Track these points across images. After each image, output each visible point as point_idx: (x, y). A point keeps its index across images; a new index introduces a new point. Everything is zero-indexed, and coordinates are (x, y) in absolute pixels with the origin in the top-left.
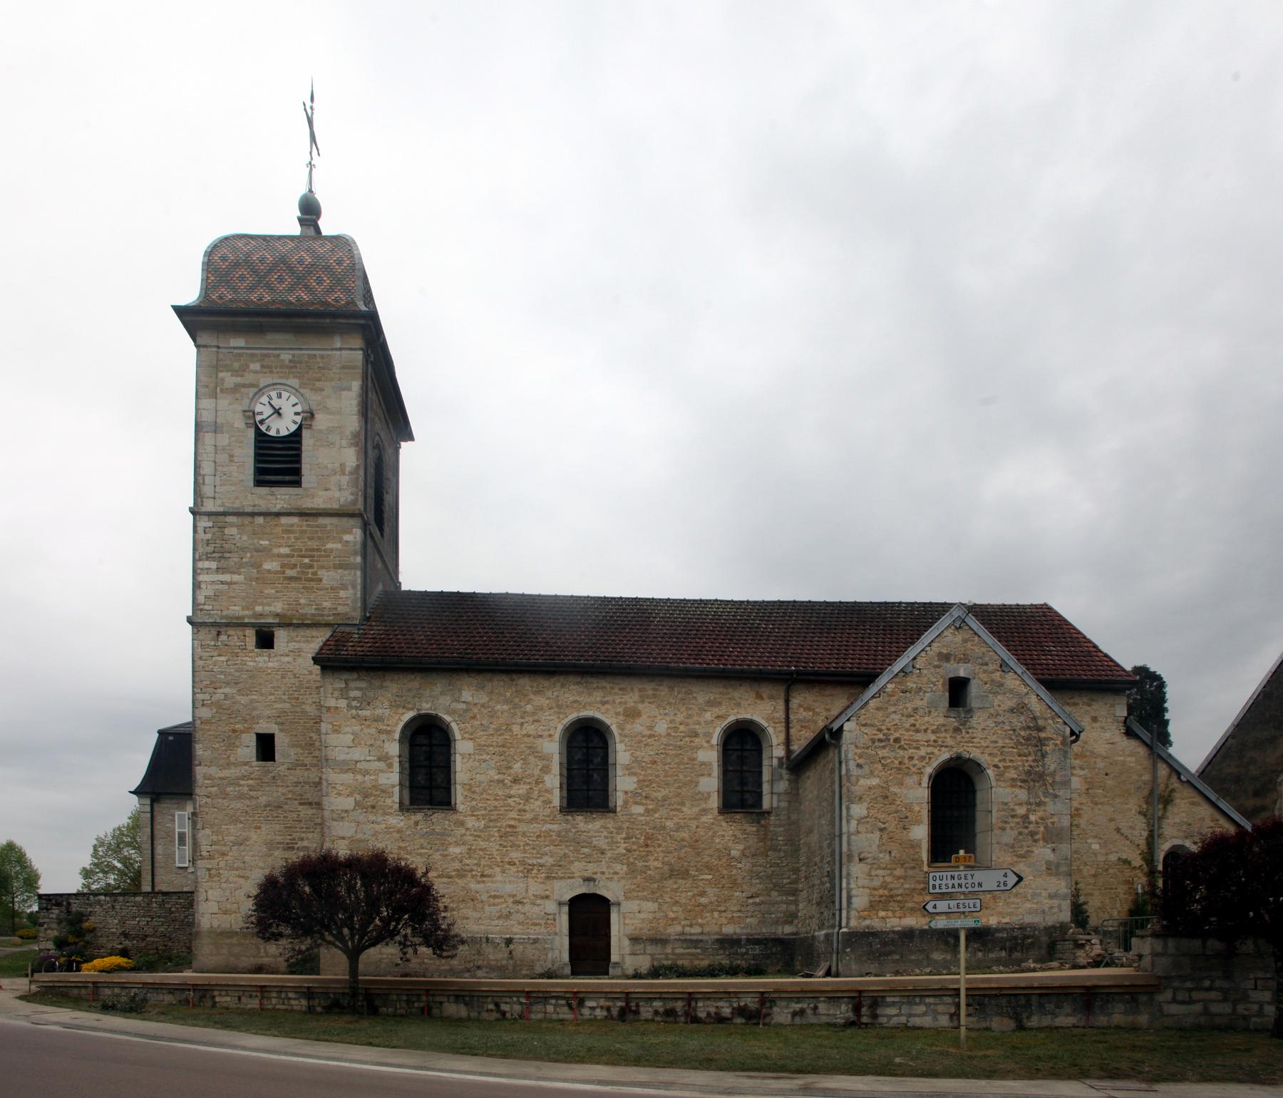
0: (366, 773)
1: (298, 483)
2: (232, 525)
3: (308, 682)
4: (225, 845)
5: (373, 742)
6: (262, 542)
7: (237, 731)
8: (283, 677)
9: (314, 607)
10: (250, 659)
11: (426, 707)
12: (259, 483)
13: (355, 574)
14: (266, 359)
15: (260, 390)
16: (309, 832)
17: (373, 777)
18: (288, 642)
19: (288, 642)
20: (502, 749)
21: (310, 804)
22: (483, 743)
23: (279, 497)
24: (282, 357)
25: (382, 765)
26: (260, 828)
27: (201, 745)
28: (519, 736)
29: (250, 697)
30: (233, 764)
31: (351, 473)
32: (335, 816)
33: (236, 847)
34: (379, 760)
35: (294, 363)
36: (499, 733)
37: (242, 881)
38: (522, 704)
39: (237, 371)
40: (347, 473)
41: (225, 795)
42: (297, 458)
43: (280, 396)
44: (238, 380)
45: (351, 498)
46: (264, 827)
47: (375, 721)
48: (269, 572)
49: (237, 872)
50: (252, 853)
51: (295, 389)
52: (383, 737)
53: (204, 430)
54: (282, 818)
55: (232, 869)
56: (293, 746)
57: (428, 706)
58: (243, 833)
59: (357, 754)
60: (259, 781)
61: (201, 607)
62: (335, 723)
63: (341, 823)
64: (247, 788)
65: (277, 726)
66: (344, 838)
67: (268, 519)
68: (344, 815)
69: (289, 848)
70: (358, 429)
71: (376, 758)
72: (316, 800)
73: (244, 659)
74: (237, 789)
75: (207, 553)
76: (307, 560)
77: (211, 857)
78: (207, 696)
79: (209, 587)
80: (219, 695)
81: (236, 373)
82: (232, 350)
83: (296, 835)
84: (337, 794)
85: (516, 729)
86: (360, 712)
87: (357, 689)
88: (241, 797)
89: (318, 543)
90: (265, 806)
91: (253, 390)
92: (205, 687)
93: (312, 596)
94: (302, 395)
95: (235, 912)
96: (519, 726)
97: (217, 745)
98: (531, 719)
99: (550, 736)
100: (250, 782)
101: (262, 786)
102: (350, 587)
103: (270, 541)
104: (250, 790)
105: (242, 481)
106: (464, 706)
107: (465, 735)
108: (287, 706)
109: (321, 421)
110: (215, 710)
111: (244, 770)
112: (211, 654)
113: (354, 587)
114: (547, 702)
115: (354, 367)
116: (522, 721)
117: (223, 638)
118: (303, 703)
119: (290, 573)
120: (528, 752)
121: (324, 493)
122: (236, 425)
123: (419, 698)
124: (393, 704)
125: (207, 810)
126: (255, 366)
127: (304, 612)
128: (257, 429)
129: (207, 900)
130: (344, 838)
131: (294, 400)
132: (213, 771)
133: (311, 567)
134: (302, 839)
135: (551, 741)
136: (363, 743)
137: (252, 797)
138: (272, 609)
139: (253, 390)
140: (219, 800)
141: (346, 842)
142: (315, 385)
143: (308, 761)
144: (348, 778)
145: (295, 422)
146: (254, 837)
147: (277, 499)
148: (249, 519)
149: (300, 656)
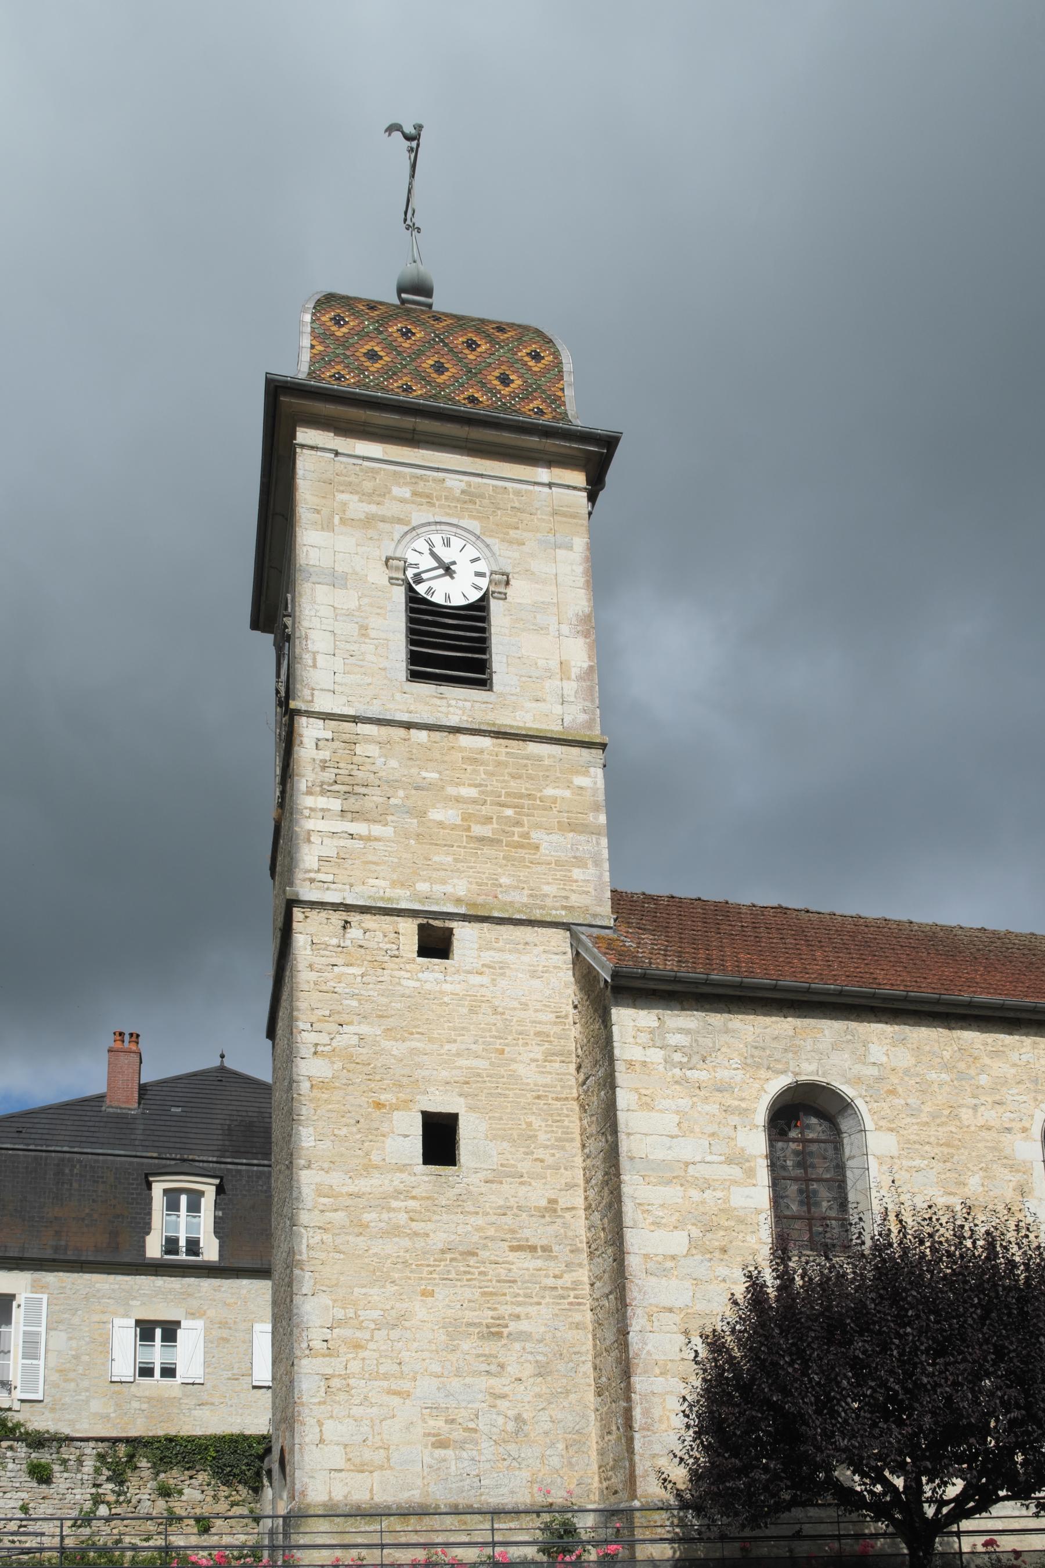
0: (706, 1185)
1: (484, 684)
2: (369, 739)
3: (520, 1022)
4: (360, 1328)
5: (713, 1128)
6: (424, 774)
7: (384, 1106)
8: (472, 1011)
9: (526, 892)
10: (408, 975)
11: (809, 1072)
12: (415, 676)
13: (598, 844)
14: (422, 483)
15: (414, 529)
16: (531, 1304)
17: (719, 1194)
18: (480, 949)
19: (480, 949)
20: (946, 1150)
21: (533, 1249)
22: (913, 1137)
23: (453, 702)
24: (449, 483)
25: (735, 1172)
26: (432, 1294)
27: (311, 1129)
28: (973, 1128)
29: (408, 1044)
30: (377, 1167)
31: (579, 678)
32: (651, 1265)
33: (384, 1332)
34: (729, 1161)
35: (470, 497)
36: (938, 1121)
37: (396, 1401)
38: (972, 1072)
39: (370, 495)
40: (573, 677)
41: (361, 1228)
42: (482, 644)
43: (447, 543)
44: (373, 508)
45: (583, 717)
46: (441, 1293)
47: (719, 1090)
48: (441, 824)
49: (385, 1384)
50: (416, 1344)
51: (474, 535)
52: (734, 1120)
53: (313, 579)
54: (476, 1276)
55: (376, 1376)
56: (495, 1138)
57: (813, 1067)
58: (398, 1305)
59: (688, 1149)
60: (429, 1202)
61: (312, 875)
62: (643, 1091)
63: (664, 1280)
64: (406, 1216)
65: (462, 1100)
66: (671, 1310)
67: (437, 735)
68: (669, 1264)
69: (493, 1334)
70: (587, 610)
71: (723, 1158)
72: (544, 1242)
73: (397, 973)
74: (385, 1216)
75: (322, 783)
76: (509, 812)
77: (330, 1353)
78: (324, 1038)
79: (326, 841)
80: (347, 1038)
81: (368, 497)
82: (360, 462)
83: (505, 1310)
84: (653, 1223)
85: (966, 1114)
86: (689, 1073)
87: (680, 1031)
88: (394, 1231)
89: (528, 786)
90: (443, 1252)
91: (400, 529)
92: (319, 1021)
93: (523, 874)
94: (488, 546)
95: (381, 1468)
96: (970, 1111)
97: (344, 1131)
98: (989, 1100)
99: (1024, 1130)
100: (412, 1204)
101: (434, 1212)
102: (590, 863)
103: (440, 773)
104: (412, 1220)
105: (385, 669)
106: (874, 1071)
107: (882, 1123)
108: (482, 1064)
109: (519, 590)
110: (338, 1065)
111: (398, 1180)
112: (333, 961)
113: (597, 863)
114: (1013, 1071)
115: (574, 516)
116: (975, 1101)
117: (354, 933)
118: (514, 1060)
119: (478, 830)
120: (990, 1157)
121: (534, 705)
122: (370, 579)
123: (795, 1053)
124: (749, 1061)
125: (323, 1256)
126: (405, 492)
127: (509, 899)
128: (410, 589)
129: (322, 1441)
130: (671, 1310)
131: (471, 552)
132: (336, 1179)
133: (518, 823)
134: (518, 1317)
135: (1026, 1139)
136: (697, 1129)
137: (416, 1234)
138: (449, 889)
139: (400, 529)
140: (351, 1238)
141: (677, 1318)
142: (507, 534)
143: (524, 1167)
144: (672, 1193)
145: (478, 588)
146: (420, 1310)
147: (449, 706)
148: (401, 732)
149: (502, 974)
